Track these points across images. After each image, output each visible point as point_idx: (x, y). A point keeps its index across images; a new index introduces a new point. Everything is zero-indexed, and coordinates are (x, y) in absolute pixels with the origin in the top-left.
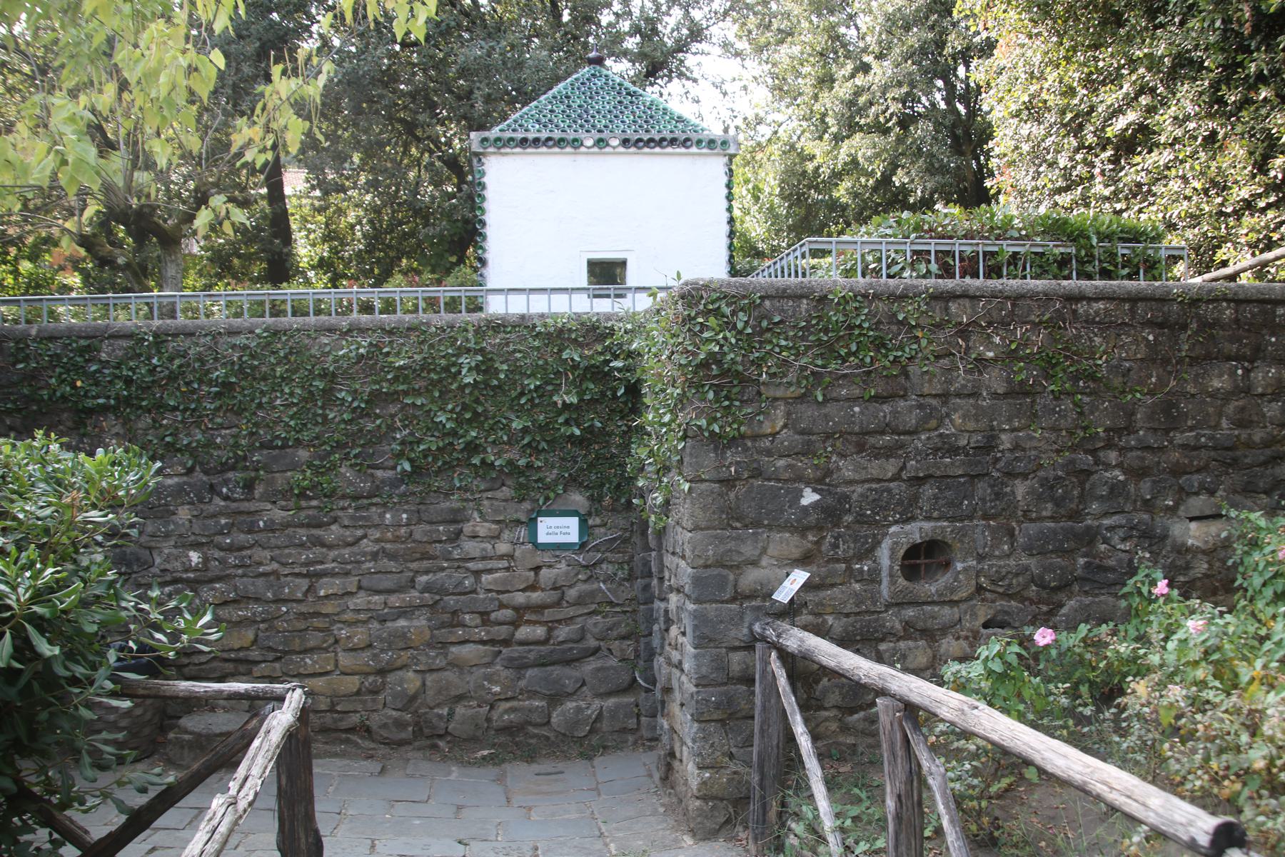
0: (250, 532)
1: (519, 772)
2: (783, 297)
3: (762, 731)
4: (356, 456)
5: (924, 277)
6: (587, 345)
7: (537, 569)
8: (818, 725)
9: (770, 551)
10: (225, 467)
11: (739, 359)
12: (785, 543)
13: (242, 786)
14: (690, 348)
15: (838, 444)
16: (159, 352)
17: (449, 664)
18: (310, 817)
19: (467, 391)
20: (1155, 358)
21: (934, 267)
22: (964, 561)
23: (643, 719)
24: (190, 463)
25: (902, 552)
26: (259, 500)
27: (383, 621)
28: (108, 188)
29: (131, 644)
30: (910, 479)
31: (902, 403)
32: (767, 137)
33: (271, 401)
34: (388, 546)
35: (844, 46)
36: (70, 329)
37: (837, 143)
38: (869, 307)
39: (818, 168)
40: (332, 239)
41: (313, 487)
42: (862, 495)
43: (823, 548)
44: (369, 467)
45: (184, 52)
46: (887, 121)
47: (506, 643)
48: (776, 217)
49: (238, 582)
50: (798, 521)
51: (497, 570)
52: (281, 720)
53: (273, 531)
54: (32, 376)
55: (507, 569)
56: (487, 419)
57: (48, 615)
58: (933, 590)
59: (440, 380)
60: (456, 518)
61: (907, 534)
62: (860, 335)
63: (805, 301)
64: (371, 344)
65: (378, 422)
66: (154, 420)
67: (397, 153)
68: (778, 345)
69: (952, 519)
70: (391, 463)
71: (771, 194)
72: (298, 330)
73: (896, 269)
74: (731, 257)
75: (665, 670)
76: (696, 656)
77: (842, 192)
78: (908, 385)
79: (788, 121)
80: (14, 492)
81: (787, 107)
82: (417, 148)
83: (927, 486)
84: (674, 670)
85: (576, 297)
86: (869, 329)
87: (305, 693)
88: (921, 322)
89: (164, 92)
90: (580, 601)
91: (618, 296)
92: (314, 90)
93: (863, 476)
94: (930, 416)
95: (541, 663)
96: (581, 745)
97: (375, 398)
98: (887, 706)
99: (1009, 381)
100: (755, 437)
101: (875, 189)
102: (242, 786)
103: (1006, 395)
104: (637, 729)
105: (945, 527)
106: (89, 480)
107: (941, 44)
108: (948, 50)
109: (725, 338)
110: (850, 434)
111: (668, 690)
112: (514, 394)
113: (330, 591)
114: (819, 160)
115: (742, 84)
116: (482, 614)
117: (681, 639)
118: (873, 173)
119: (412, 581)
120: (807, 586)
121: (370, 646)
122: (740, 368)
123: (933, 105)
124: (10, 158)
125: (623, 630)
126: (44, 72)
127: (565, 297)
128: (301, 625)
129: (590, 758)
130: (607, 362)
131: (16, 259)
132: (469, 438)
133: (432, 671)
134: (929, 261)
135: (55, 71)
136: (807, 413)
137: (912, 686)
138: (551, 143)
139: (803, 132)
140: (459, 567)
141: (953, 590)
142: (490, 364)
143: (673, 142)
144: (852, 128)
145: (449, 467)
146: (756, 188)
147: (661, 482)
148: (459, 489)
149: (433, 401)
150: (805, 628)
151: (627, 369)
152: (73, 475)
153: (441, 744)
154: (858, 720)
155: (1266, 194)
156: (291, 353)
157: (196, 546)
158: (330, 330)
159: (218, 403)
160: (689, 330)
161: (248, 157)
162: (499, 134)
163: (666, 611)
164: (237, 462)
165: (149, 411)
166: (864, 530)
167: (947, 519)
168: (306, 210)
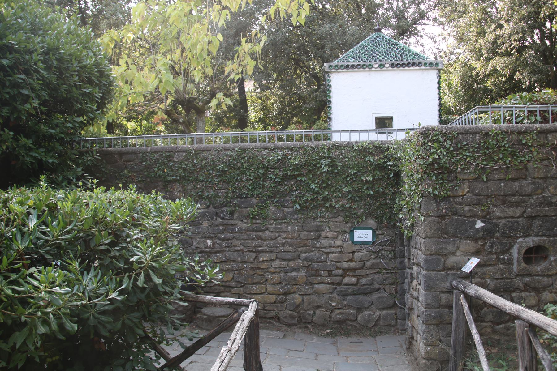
0: (232, 233)
1: (343, 341)
2: (468, 134)
3: (456, 331)
4: (276, 202)
5: (534, 123)
6: (377, 155)
7: (353, 253)
8: (481, 329)
9: (460, 249)
10: (222, 206)
11: (447, 161)
12: (467, 245)
13: (233, 343)
14: (425, 157)
15: (493, 200)
16: (197, 158)
17: (314, 292)
18: (257, 357)
19: (324, 175)
21: (538, 118)
22: (554, 256)
23: (399, 321)
24: (208, 203)
25: (524, 251)
26: (236, 220)
27: (286, 272)
28: (177, 91)
29: (187, 279)
30: (528, 217)
31: (524, 182)
32: (454, 60)
33: (241, 179)
34: (289, 240)
35: (490, 17)
36: (162, 148)
37: (487, 61)
38: (508, 137)
39: (477, 73)
40: (264, 110)
41: (258, 215)
42: (504, 224)
43: (486, 248)
44: (282, 206)
45: (207, 35)
46: (512, 50)
47: (339, 284)
48: (459, 96)
49: (226, 253)
50: (474, 235)
51: (336, 252)
52: (248, 315)
53: (241, 233)
54: (148, 167)
55: (340, 252)
56: (332, 187)
57: (157, 267)
58: (539, 269)
59: (313, 170)
60: (319, 229)
61: (526, 243)
62: (504, 150)
63: (478, 135)
64: (283, 154)
65: (286, 188)
66: (194, 186)
67: (291, 73)
68: (465, 155)
69: (549, 236)
70: (291, 205)
71: (457, 86)
72: (253, 149)
73: (520, 119)
74: (440, 115)
75: (410, 300)
76: (425, 295)
77: (489, 84)
78: (527, 173)
79: (464, 52)
80: (144, 215)
81: (463, 46)
82: (300, 70)
83: (536, 221)
84: (414, 300)
85: (371, 134)
86: (509, 147)
87: (257, 304)
88: (534, 144)
89: (199, 52)
90: (371, 268)
91: (389, 133)
92: (259, 48)
93: (505, 215)
94: (538, 188)
95: (354, 294)
96: (371, 331)
97: (285, 177)
98: (520, 325)
100: (454, 197)
101: (505, 82)
102: (233, 343)
104: (396, 325)
105: (545, 240)
106: (174, 212)
107: (538, 13)
108: (541, 16)
109: (441, 152)
110: (499, 196)
111: (411, 309)
112: (344, 176)
113: (265, 259)
114: (478, 69)
115: (443, 37)
116: (329, 271)
117: (418, 287)
118: (505, 74)
119: (299, 256)
120: (478, 265)
121: (280, 283)
122: (448, 166)
123: (534, 41)
124: (142, 81)
125: (391, 281)
126: (154, 47)
127: (366, 134)
129: (374, 337)
130: (386, 162)
131: (141, 120)
132: (324, 195)
133: (306, 295)
134: (536, 115)
135: (157, 46)
136: (479, 186)
137: (534, 316)
138: (359, 67)
139: (471, 57)
140: (319, 251)
141: (549, 270)
142: (334, 163)
143: (413, 64)
144: (494, 53)
145: (316, 207)
146: (449, 83)
147: (410, 216)
148: (320, 217)
149: (309, 179)
150: (477, 284)
151: (394, 165)
152: (167, 209)
153: (309, 326)
154: (501, 328)
156: (250, 158)
157: (210, 238)
158: (266, 149)
159: (220, 179)
160: (425, 148)
161: (232, 77)
162: (337, 64)
163: (411, 274)
164: (227, 204)
165: (192, 182)
166: (505, 240)
167: (546, 236)
168: (254, 97)
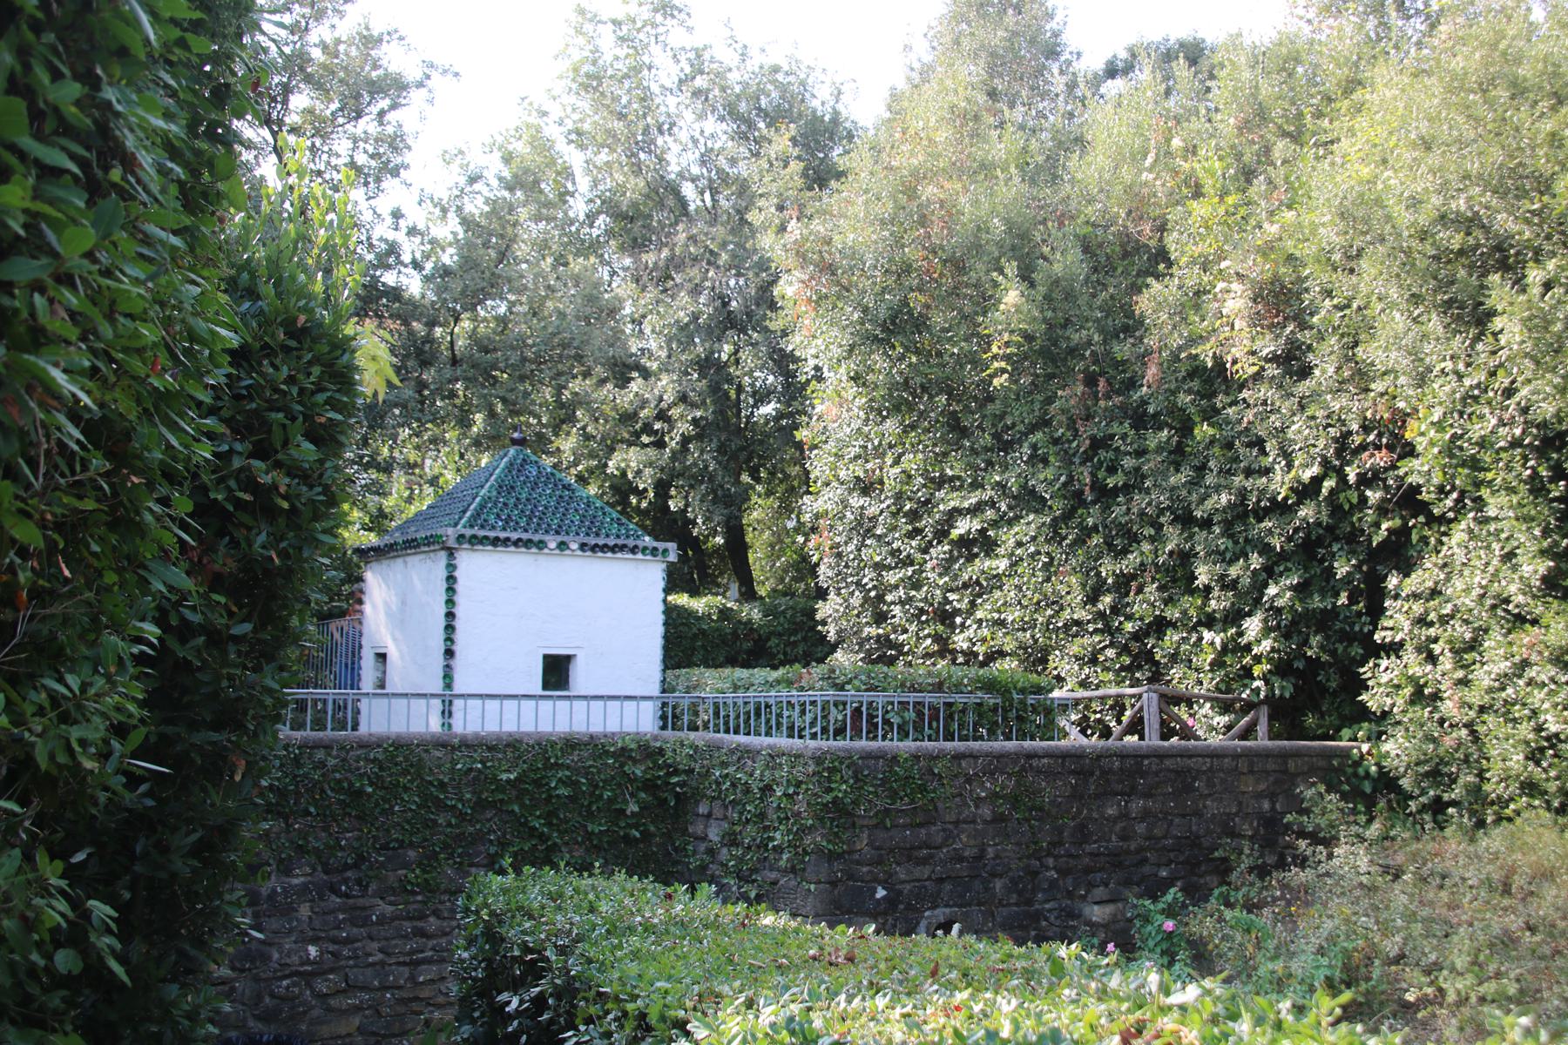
20: (1076, 795)
69: (960, 906)
99: (993, 812)
103: (992, 821)
128: (401, 1009)
136: (881, 835)
155: (1094, 621)
157: (314, 941)
